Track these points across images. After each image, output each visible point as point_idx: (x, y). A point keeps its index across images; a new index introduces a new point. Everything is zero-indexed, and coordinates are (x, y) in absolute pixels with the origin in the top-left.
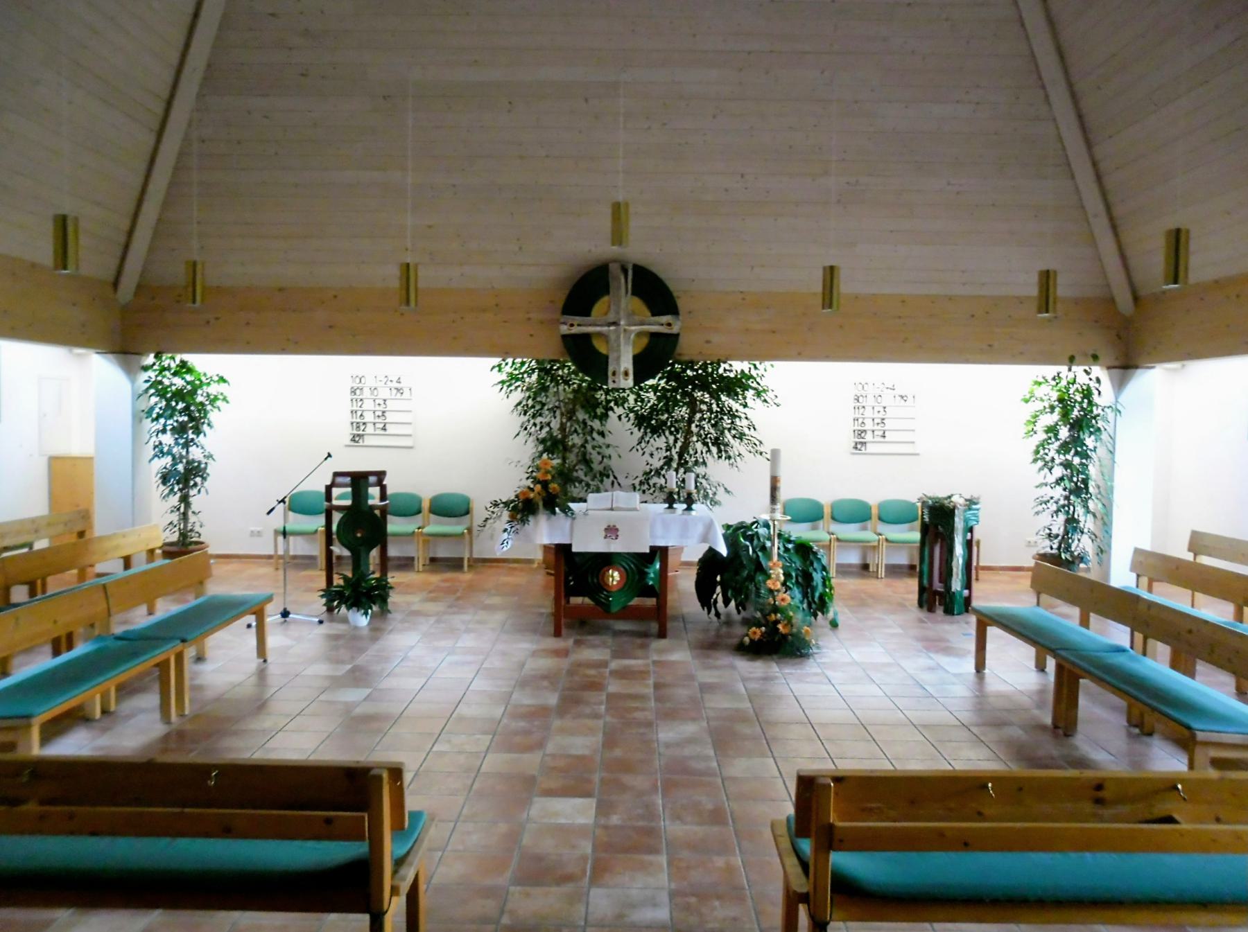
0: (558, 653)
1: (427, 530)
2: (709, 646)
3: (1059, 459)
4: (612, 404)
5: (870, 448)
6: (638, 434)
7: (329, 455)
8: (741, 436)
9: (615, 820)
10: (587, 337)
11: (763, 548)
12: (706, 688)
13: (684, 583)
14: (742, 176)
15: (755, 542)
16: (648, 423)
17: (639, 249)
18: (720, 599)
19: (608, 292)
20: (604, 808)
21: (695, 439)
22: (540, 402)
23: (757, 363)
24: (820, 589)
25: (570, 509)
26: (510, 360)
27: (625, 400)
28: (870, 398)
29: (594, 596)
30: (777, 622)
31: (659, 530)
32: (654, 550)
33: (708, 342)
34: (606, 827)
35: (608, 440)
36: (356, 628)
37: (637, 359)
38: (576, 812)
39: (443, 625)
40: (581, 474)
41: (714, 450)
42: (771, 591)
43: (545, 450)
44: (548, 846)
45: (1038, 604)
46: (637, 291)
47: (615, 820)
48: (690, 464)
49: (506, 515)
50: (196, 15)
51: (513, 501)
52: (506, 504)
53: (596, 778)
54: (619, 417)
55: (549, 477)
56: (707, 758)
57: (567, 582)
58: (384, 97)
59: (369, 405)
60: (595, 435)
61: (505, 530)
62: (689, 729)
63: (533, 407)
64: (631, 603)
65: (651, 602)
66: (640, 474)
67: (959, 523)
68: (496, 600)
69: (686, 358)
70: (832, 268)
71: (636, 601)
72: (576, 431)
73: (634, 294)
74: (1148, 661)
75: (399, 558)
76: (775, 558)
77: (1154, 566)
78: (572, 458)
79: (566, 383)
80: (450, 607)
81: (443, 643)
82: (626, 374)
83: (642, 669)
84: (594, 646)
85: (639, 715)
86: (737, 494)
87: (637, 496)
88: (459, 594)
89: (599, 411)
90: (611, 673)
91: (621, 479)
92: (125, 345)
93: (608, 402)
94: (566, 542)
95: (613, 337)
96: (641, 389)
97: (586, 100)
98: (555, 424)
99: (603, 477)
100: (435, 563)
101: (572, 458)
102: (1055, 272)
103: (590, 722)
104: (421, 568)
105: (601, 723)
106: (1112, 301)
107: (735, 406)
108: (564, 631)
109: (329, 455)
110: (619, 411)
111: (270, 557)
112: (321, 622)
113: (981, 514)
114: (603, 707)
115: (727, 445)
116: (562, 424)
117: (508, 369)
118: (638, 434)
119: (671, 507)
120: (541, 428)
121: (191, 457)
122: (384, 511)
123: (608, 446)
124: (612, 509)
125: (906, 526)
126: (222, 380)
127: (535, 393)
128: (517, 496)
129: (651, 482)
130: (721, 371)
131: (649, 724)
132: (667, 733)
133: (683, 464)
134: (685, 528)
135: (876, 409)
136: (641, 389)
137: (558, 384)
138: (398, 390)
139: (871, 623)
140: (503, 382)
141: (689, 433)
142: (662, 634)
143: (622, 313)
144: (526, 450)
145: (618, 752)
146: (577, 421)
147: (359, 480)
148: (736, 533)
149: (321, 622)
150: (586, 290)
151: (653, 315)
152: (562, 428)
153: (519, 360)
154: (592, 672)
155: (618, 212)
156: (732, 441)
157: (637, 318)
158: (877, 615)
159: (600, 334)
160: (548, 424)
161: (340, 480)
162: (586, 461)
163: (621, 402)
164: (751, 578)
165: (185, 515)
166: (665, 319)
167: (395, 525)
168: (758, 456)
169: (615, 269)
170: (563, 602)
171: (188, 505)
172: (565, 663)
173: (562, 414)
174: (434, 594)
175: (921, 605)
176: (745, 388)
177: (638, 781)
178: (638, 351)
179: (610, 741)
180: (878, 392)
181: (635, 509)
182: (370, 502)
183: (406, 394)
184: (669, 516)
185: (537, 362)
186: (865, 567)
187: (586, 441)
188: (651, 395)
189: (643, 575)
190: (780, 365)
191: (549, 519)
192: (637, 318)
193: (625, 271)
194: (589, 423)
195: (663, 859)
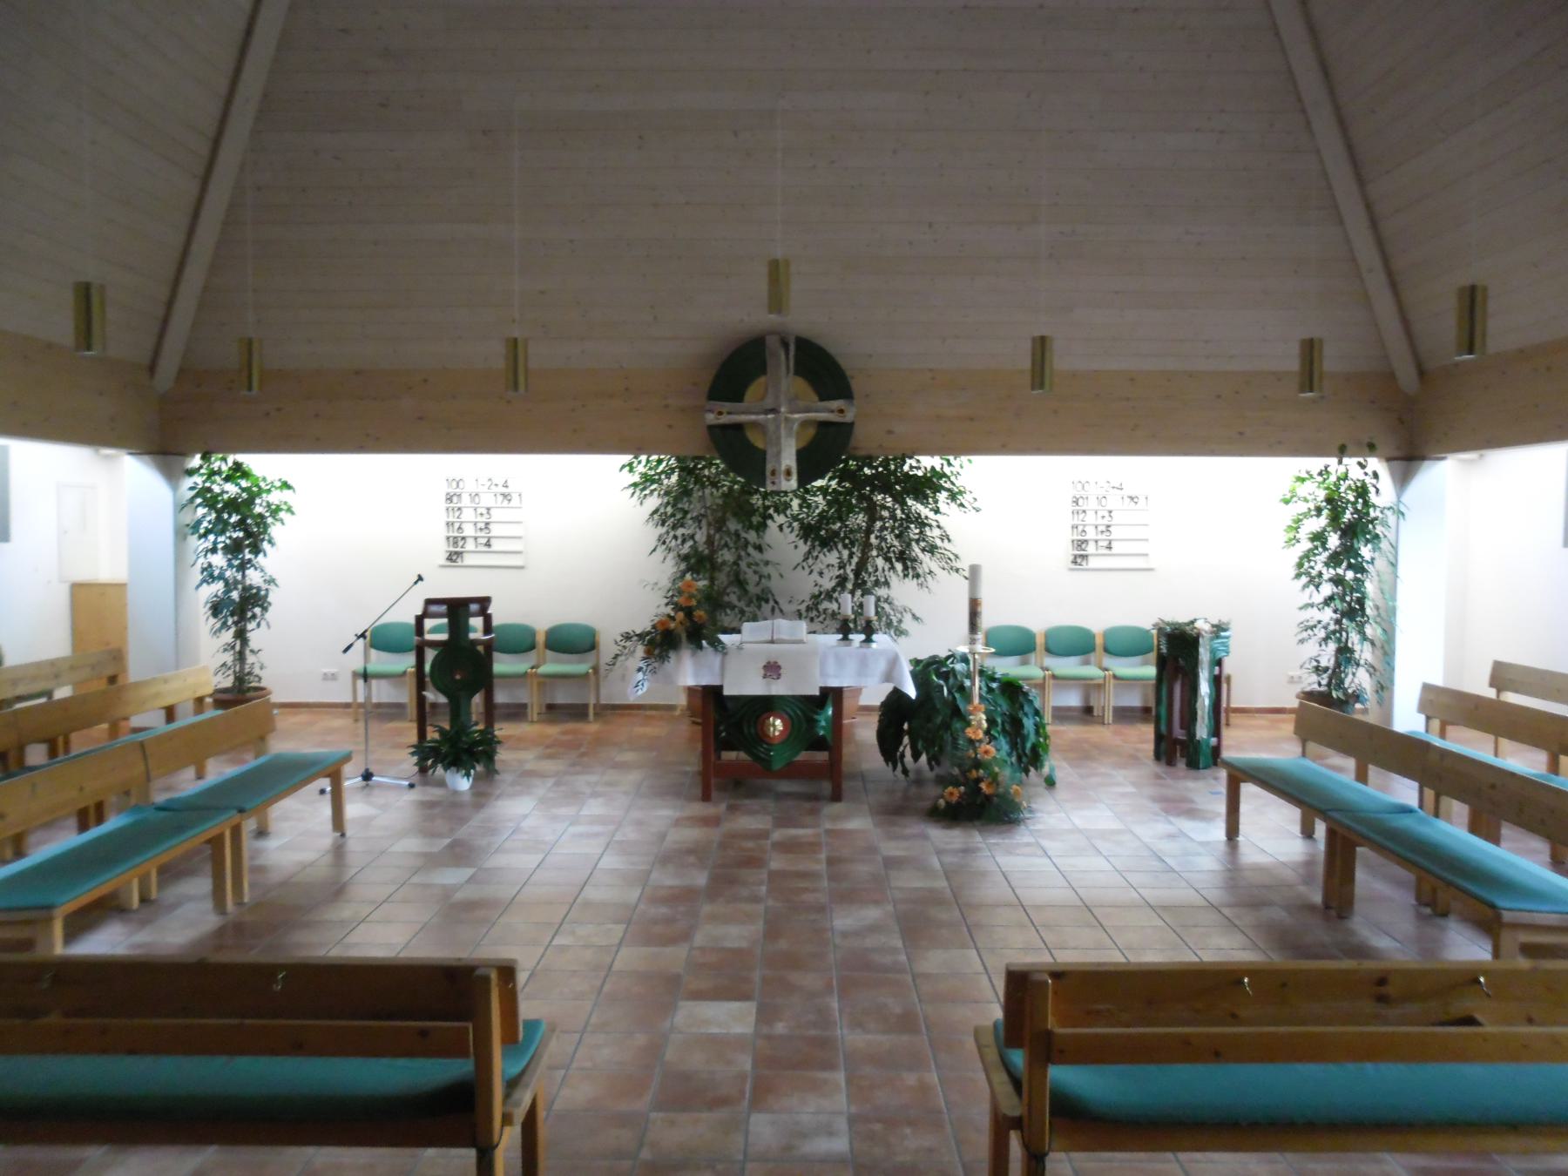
0: (707, 822)
2: (895, 811)
3: (1328, 573)
5: (1093, 562)
6: (804, 548)
8: (932, 549)
9: (780, 1028)
10: (739, 427)
11: (962, 688)
12: (891, 863)
13: (865, 732)
14: (930, 225)
15: (951, 681)
16: (817, 534)
17: (803, 318)
18: (908, 753)
19: (763, 371)
20: (766, 1015)
21: (874, 553)
23: (951, 458)
24: (1032, 738)
25: (720, 642)
27: (787, 506)
29: (749, 751)
30: (979, 780)
31: (831, 667)
33: (890, 432)
34: (769, 1038)
35: (768, 555)
36: (456, 793)
37: (802, 455)
38: (731, 1018)
40: (733, 598)
42: (971, 742)
44: (696, 1061)
45: (1304, 754)
47: (780, 1028)
49: (640, 650)
50: (249, 32)
51: (648, 633)
52: (641, 636)
53: (756, 976)
54: (781, 527)
56: (894, 950)
57: (717, 734)
58: (484, 133)
59: (468, 515)
60: (750, 550)
61: (640, 670)
62: (872, 914)
63: (673, 515)
65: (822, 756)
67: (1204, 655)
68: (629, 756)
69: (862, 453)
70: (1043, 339)
71: (803, 756)
72: (726, 545)
73: (797, 373)
74: (1442, 825)
77: (1445, 705)
78: (722, 578)
79: (714, 485)
80: (574, 765)
81: (563, 811)
82: (788, 473)
85: (808, 897)
86: (932, 618)
87: (803, 625)
89: (756, 519)
92: (164, 447)
93: (767, 508)
94: (714, 681)
95: (771, 428)
96: (807, 491)
97: (736, 134)
98: (701, 537)
100: (554, 712)
101: (722, 578)
102: (1321, 341)
103: (748, 907)
104: (535, 717)
105: (761, 908)
106: (1391, 376)
107: (924, 511)
108: (714, 794)
110: (780, 519)
111: (347, 706)
112: (412, 786)
113: (1231, 643)
115: (914, 560)
117: (641, 469)
118: (804, 548)
119: (845, 638)
120: (684, 542)
121: (248, 582)
122: (489, 647)
123: (767, 563)
124: (772, 642)
125: (1138, 659)
126: (286, 486)
128: (654, 627)
129: (821, 607)
130: (906, 468)
131: (821, 909)
132: (844, 920)
133: (860, 584)
134: (863, 664)
135: (1100, 514)
136: (807, 491)
138: (505, 496)
140: (635, 485)
141: (867, 546)
142: (836, 797)
144: (664, 569)
145: (783, 944)
146: (728, 533)
147: (457, 609)
148: (926, 670)
149: (412, 786)
150: (737, 369)
151: (822, 399)
152: (710, 541)
154: (750, 844)
155: (777, 272)
157: (801, 404)
158: (1103, 770)
159: (755, 424)
160: (692, 537)
161: (434, 608)
163: (783, 508)
164: (946, 726)
166: (835, 404)
167: (502, 665)
168: (954, 574)
169: (772, 343)
172: (715, 834)
173: (709, 525)
174: (552, 750)
176: (939, 489)
177: (809, 980)
178: (802, 444)
179: (773, 931)
180: (1102, 493)
181: (801, 642)
182: (472, 636)
183: (515, 501)
184: (844, 650)
186: (1088, 710)
187: (739, 557)
188: (820, 499)
189: (812, 722)
191: (693, 655)
192: (801, 404)
193: (785, 345)
195: (840, 1077)
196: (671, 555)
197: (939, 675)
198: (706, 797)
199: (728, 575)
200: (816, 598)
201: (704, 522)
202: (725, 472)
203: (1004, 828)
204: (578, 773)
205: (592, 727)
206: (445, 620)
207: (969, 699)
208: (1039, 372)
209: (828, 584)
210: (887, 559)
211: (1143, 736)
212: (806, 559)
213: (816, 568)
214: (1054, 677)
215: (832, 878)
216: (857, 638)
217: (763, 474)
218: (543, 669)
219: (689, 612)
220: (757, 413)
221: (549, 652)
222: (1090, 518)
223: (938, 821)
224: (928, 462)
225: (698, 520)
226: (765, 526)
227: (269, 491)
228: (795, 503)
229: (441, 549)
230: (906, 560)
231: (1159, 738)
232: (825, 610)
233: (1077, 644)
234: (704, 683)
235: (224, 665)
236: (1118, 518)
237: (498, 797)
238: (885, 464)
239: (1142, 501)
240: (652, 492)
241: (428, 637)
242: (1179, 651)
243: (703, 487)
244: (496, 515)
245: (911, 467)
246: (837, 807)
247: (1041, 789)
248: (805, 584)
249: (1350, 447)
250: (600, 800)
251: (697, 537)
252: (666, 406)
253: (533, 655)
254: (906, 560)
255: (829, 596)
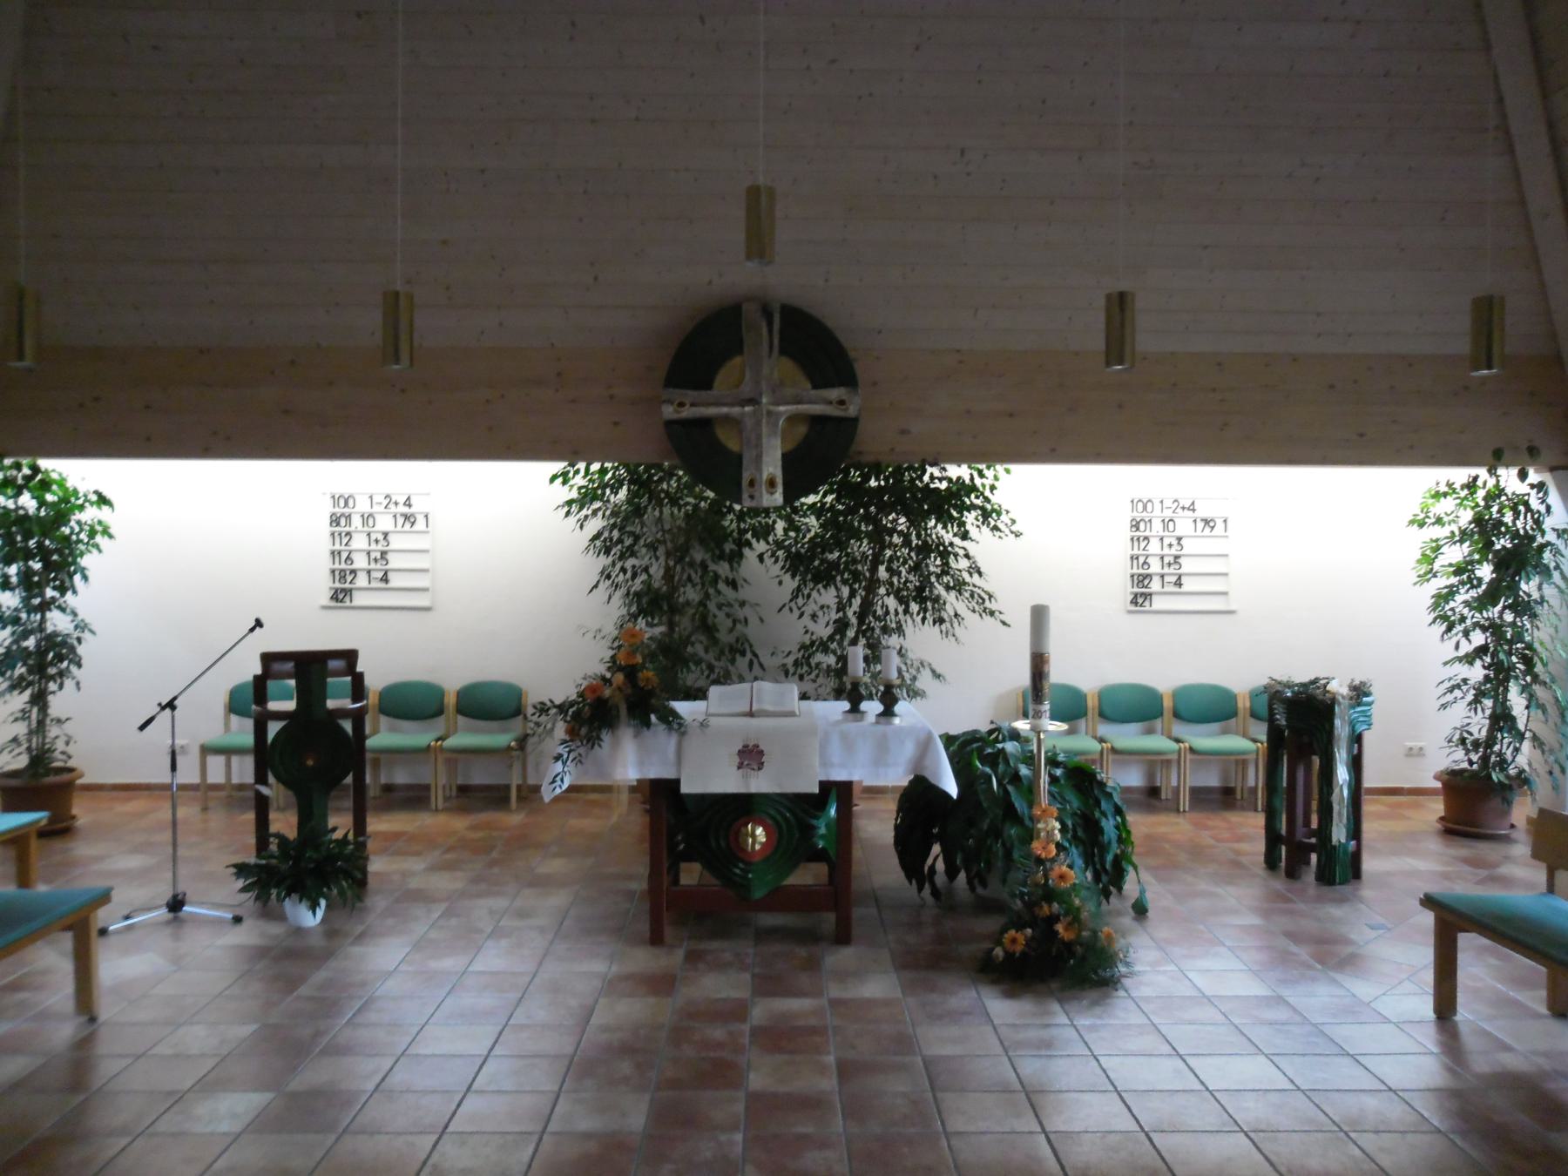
0: (660, 984)
1: (451, 742)
2: (930, 961)
3: (1473, 617)
4: (749, 536)
5: (1158, 603)
6: (790, 583)
7: (259, 624)
8: (958, 586)
10: (705, 423)
11: (1016, 778)
13: (877, 827)
14: (963, 152)
15: (1001, 768)
16: (810, 566)
17: (790, 277)
18: (940, 866)
19: (740, 351)
21: (882, 591)
22: (632, 534)
23: (982, 466)
24: (1115, 849)
26: (582, 466)
27: (770, 529)
28: (1157, 526)
29: (721, 875)
30: (1054, 919)
31: (835, 749)
32: (826, 786)
33: (904, 432)
35: (743, 594)
36: (299, 931)
37: (788, 460)
39: (454, 921)
40: (699, 649)
41: (914, 607)
42: (1040, 861)
43: (642, 612)
45: (1551, 888)
46: (789, 348)
48: (877, 631)
49: (560, 730)
51: (572, 704)
52: (562, 708)
54: (761, 557)
55: (639, 659)
58: (359, 15)
59: (359, 542)
60: (721, 586)
61: (558, 758)
63: (620, 541)
64: (792, 880)
66: (795, 648)
67: (1341, 729)
68: (555, 866)
69: (869, 458)
72: (689, 579)
75: (409, 787)
76: (1044, 799)
78: (685, 623)
79: (674, 501)
80: (476, 880)
81: (449, 963)
82: (772, 484)
83: (813, 1021)
84: (720, 967)
86: (959, 679)
87: (794, 689)
88: (495, 854)
89: (729, 547)
90: (757, 1032)
91: (765, 659)
93: (742, 532)
94: (668, 774)
95: (749, 423)
96: (795, 511)
97: (702, 19)
98: (657, 571)
99: (732, 657)
100: (469, 797)
101: (685, 623)
104: (440, 805)
107: (948, 537)
108: (668, 931)
109: (259, 624)
110: (761, 546)
112: (238, 920)
113: (1375, 711)
114: (739, 1137)
115: (936, 600)
116: (668, 569)
117: (579, 481)
118: (790, 583)
119: (855, 709)
120: (634, 576)
121: (50, 628)
123: (742, 604)
124: (751, 714)
125: (1215, 726)
126: (103, 500)
127: (626, 519)
128: (581, 695)
129: (813, 662)
130: (926, 478)
133: (864, 631)
134: (882, 752)
135: (1166, 541)
136: (795, 511)
137: (660, 504)
138: (407, 517)
139: (1200, 903)
140: (570, 503)
141: (873, 585)
142: (843, 937)
143: (764, 385)
144: (607, 612)
146: (692, 564)
147: (309, 668)
148: (964, 749)
149: (238, 920)
150: (703, 346)
151: (815, 387)
152: (668, 575)
153: (595, 467)
154: (718, 1033)
155: (758, 208)
156: (943, 592)
158: (1203, 886)
159: (727, 419)
160: (646, 570)
161: (277, 667)
162: (707, 628)
163: (764, 532)
164: (996, 833)
165: (41, 723)
166: (835, 393)
168: (987, 618)
169: (751, 311)
170: (666, 880)
171: (44, 708)
173: (668, 554)
175: (1271, 862)
176: (963, 508)
178: (790, 447)
180: (1168, 514)
181: (791, 714)
182: (331, 704)
183: (420, 524)
184: (852, 726)
185: (626, 466)
186: (1153, 792)
187: (707, 596)
188: (812, 521)
189: (808, 831)
190: (1018, 469)
191: (636, 736)
193: (767, 313)
194: (712, 567)
196: (619, 593)
197: (985, 759)
198: (656, 939)
199: (693, 620)
200: (808, 649)
201: (661, 551)
202: (689, 488)
203: (1094, 994)
204: (479, 896)
205: (514, 819)
206: (292, 682)
207: (1030, 791)
208: (1117, 346)
209: (823, 631)
210: (902, 600)
211: (1248, 830)
212: (794, 597)
213: (808, 610)
214: (1114, 750)
215: (855, 1110)
216: (872, 707)
217: (739, 484)
218: (453, 742)
219: (631, 672)
220: (732, 405)
221: (461, 720)
222: (1154, 547)
223: (994, 982)
224: (957, 471)
225: (652, 547)
226: (741, 556)
227: (81, 508)
228: (780, 526)
229: (323, 586)
230: (922, 597)
231: (1273, 839)
232: (818, 665)
233: (1139, 706)
234: (652, 775)
235: (15, 740)
236: (1189, 546)
237: (360, 938)
238: (898, 472)
239: (1220, 525)
240: (595, 513)
241: (273, 706)
242: (1304, 724)
243: (660, 504)
244: (396, 542)
245: (932, 478)
246: (842, 957)
247: (1127, 920)
248: (791, 631)
249: (1506, 455)
250: (504, 943)
251: (652, 571)
252: (612, 397)
253: (441, 720)
254: (922, 597)
255: (824, 647)
